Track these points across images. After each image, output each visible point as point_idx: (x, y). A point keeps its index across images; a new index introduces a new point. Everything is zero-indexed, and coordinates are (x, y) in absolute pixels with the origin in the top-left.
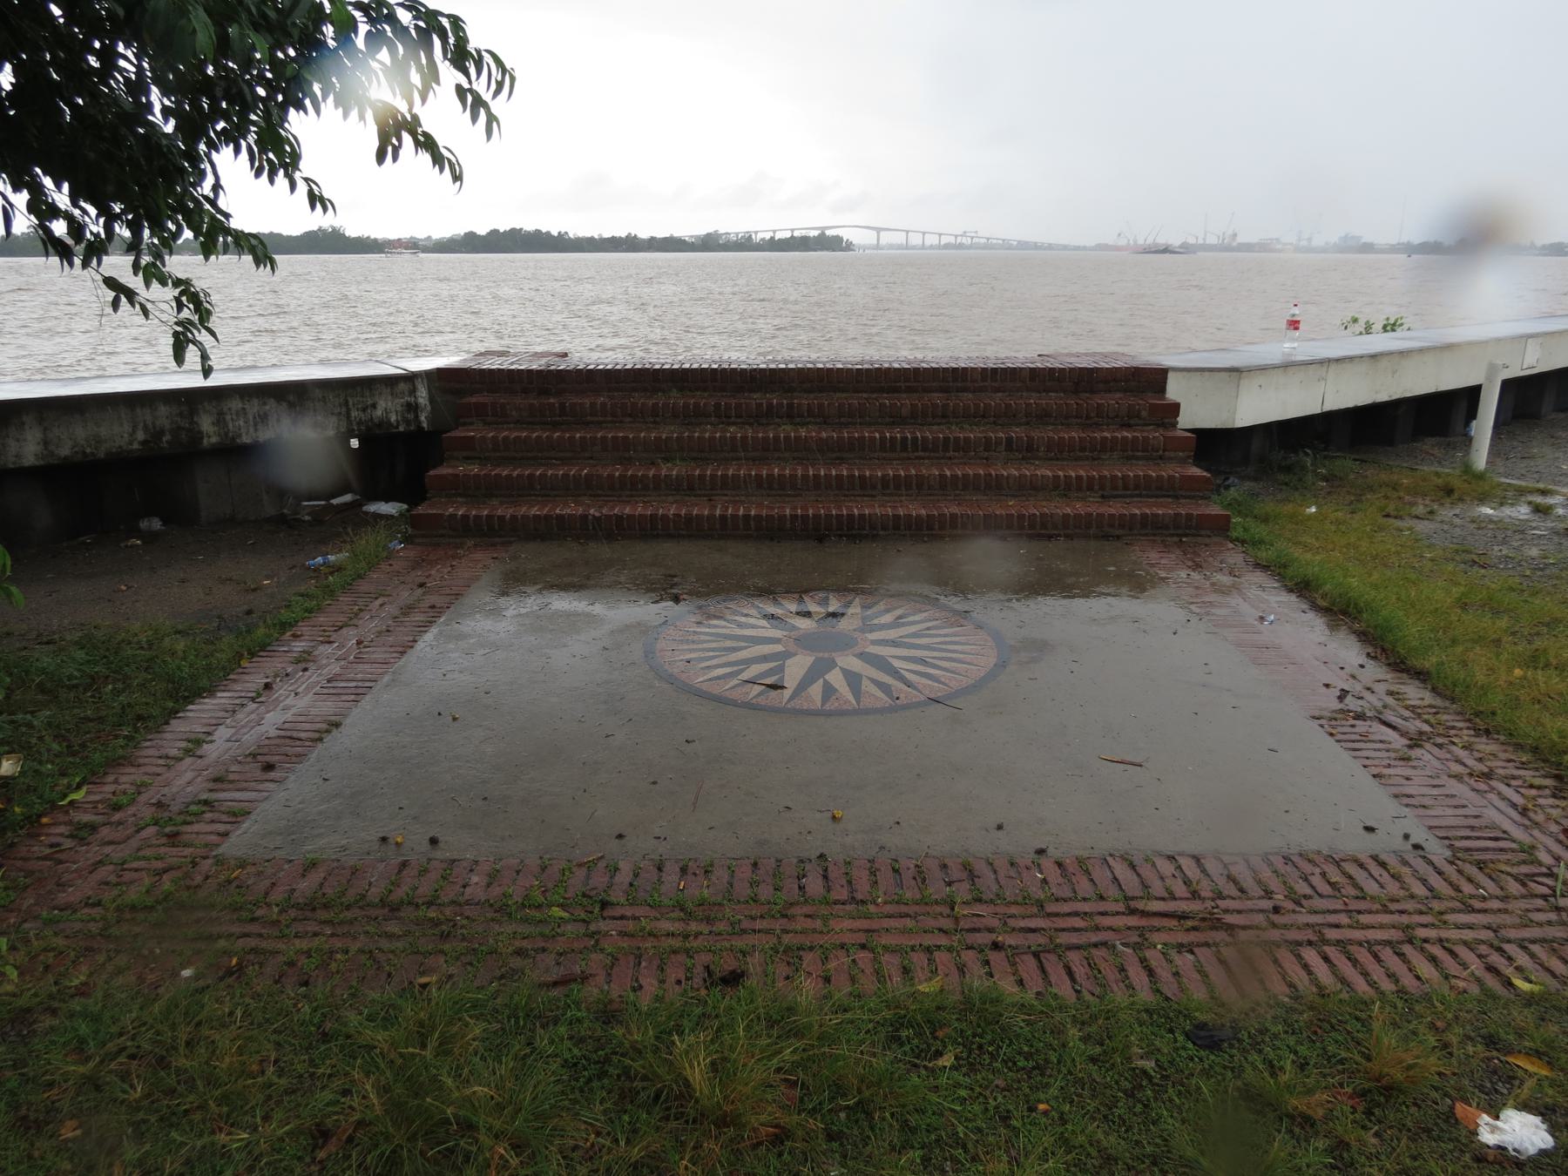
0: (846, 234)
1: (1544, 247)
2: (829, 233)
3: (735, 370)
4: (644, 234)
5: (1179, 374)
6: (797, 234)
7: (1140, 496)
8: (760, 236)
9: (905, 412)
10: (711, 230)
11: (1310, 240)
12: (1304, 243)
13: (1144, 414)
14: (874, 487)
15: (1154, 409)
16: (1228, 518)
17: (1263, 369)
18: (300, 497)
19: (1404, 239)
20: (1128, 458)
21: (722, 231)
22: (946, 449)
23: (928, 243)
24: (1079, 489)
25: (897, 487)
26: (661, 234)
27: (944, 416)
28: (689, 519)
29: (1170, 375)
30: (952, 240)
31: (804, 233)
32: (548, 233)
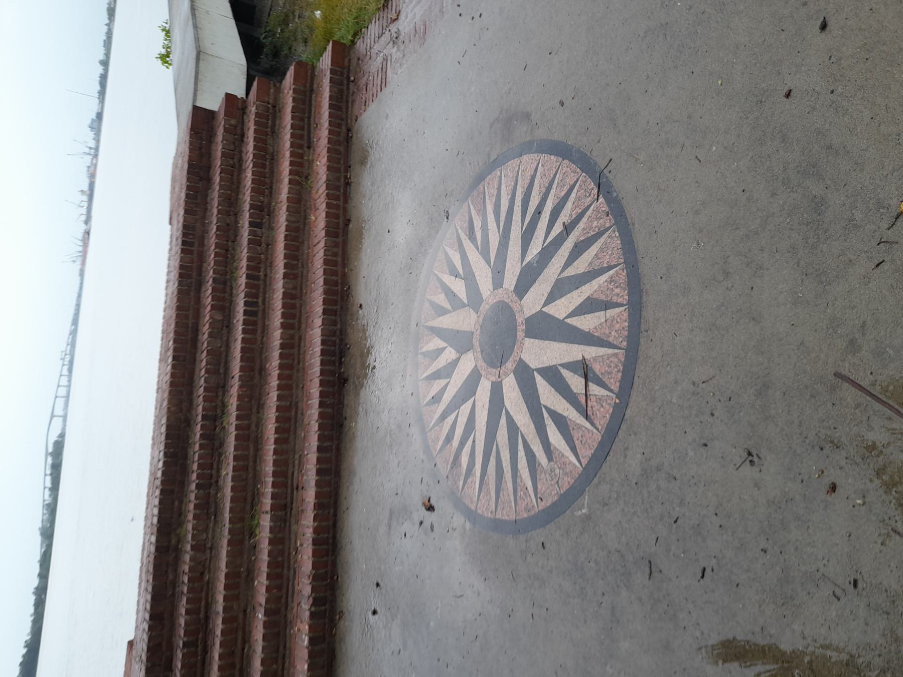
0: (53, 437)
1: (110, 19)
2: (50, 450)
3: (160, 503)
4: (35, 582)
5: (199, 97)
6: (48, 472)
7: (309, 118)
8: (47, 497)
9: (219, 317)
10: (38, 533)
11: (91, 148)
12: (92, 152)
13: (233, 122)
14: (292, 337)
15: (227, 113)
16: (334, 42)
17: (197, 39)
18: (739, 641)
19: (97, 95)
20: (273, 132)
21: (40, 525)
22: (257, 278)
23: (66, 383)
24: (301, 165)
25: (293, 316)
26: (36, 569)
27: (225, 283)
28: (318, 506)
29: (200, 104)
30: (66, 368)
31: (48, 467)
32: (24, 656)
